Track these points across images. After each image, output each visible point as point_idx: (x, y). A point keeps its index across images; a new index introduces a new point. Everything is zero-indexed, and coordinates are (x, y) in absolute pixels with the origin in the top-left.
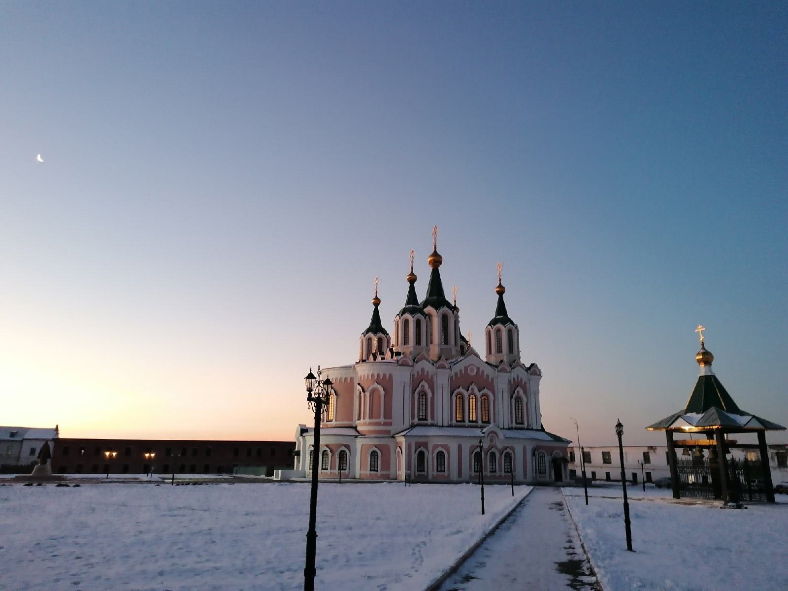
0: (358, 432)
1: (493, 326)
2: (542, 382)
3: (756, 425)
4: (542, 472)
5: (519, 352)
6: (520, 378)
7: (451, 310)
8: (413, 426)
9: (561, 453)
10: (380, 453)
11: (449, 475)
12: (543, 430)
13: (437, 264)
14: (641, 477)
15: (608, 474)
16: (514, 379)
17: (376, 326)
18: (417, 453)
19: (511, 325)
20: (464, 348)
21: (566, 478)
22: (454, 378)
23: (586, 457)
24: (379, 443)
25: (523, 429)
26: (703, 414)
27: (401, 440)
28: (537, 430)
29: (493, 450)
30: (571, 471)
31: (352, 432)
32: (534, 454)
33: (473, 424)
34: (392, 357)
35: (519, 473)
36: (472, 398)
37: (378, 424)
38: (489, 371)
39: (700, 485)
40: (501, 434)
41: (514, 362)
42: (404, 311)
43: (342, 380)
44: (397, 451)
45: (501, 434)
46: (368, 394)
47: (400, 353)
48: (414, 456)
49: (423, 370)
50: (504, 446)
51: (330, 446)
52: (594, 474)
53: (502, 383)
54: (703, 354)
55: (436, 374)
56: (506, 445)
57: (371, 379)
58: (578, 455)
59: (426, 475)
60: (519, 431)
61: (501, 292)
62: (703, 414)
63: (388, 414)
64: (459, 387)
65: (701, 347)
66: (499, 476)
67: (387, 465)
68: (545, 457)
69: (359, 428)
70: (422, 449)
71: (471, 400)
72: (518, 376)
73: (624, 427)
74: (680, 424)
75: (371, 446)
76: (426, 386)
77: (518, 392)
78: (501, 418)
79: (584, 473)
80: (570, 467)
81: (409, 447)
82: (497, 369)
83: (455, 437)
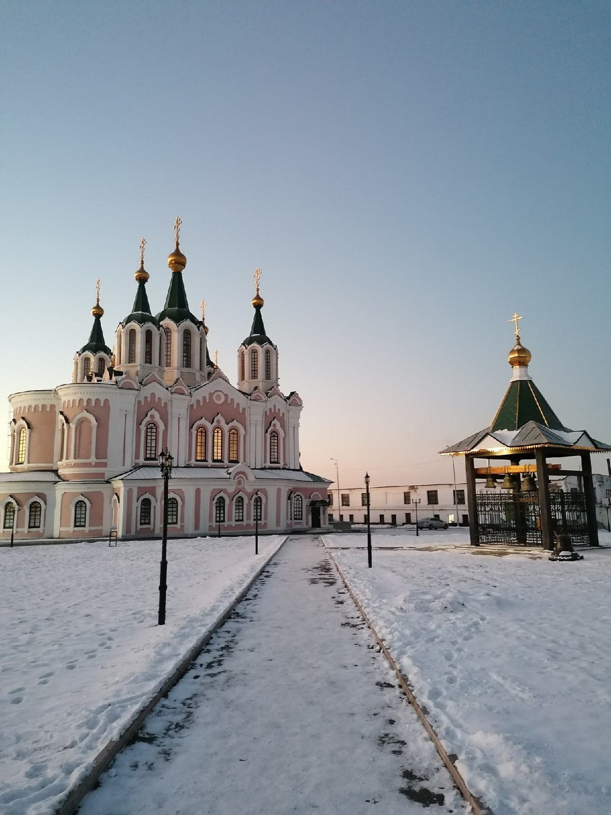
0: (59, 476)
1: (247, 346)
2: (303, 414)
3: (585, 444)
4: (298, 518)
5: (277, 379)
6: (229, 399)
7: (196, 324)
8: (137, 467)
9: (320, 495)
11: (182, 527)
12: (301, 469)
13: (180, 266)
14: (401, 518)
17: (97, 342)
18: (140, 501)
19: (269, 346)
20: (212, 371)
21: (325, 524)
22: (195, 408)
23: (345, 500)
24: (88, 490)
25: (279, 469)
26: (519, 431)
27: (118, 484)
28: (294, 470)
29: (241, 494)
30: (329, 515)
31: (51, 477)
32: (289, 498)
33: (218, 463)
34: (111, 379)
35: (270, 520)
36: (218, 432)
37: (89, 465)
38: (241, 400)
40: (251, 475)
41: (271, 390)
42: (129, 319)
43: (38, 408)
44: (113, 499)
45: (251, 475)
46: (73, 426)
47: (122, 372)
48: (137, 505)
49: (153, 395)
51: (17, 497)
52: (351, 517)
53: (256, 414)
54: (519, 351)
55: (171, 401)
57: (78, 406)
58: (337, 500)
60: (274, 471)
61: (258, 306)
62: (519, 431)
63: (101, 452)
64: (202, 418)
65: (516, 342)
67: (98, 518)
68: (302, 500)
69: (60, 472)
70: (147, 496)
71: (216, 434)
73: (370, 478)
74: (491, 445)
75: (76, 494)
77: (274, 425)
78: (253, 455)
79: (341, 517)
80: (329, 511)
81: (129, 493)
82: (249, 397)
83: (191, 479)
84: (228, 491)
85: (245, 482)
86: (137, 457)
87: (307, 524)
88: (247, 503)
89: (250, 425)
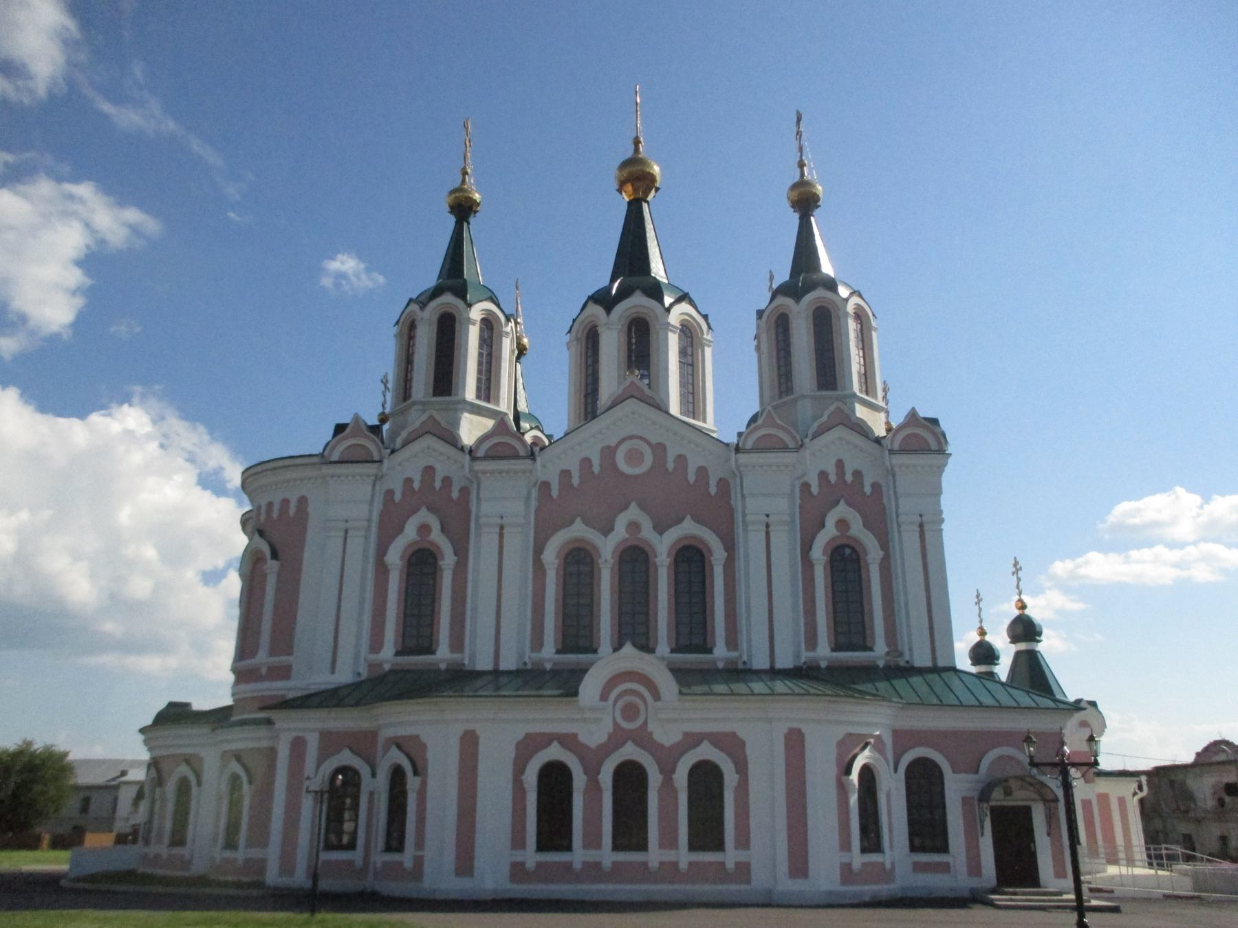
2: (950, 478)
10: (986, 757)
15: (1224, 839)
16: (823, 475)
39: (1082, 905)
49: (429, 471)
50: (686, 735)
56: (697, 728)
59: (359, 862)
66: (662, 864)
72: (840, 464)
76: (857, 528)
84: (582, 738)
85: (650, 709)
86: (376, 646)
87: (975, 868)
88: (735, 784)
89: (746, 531)
